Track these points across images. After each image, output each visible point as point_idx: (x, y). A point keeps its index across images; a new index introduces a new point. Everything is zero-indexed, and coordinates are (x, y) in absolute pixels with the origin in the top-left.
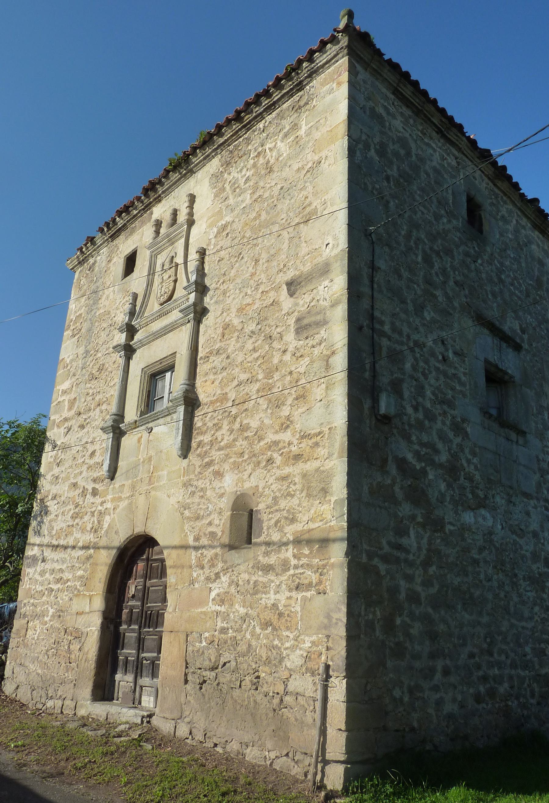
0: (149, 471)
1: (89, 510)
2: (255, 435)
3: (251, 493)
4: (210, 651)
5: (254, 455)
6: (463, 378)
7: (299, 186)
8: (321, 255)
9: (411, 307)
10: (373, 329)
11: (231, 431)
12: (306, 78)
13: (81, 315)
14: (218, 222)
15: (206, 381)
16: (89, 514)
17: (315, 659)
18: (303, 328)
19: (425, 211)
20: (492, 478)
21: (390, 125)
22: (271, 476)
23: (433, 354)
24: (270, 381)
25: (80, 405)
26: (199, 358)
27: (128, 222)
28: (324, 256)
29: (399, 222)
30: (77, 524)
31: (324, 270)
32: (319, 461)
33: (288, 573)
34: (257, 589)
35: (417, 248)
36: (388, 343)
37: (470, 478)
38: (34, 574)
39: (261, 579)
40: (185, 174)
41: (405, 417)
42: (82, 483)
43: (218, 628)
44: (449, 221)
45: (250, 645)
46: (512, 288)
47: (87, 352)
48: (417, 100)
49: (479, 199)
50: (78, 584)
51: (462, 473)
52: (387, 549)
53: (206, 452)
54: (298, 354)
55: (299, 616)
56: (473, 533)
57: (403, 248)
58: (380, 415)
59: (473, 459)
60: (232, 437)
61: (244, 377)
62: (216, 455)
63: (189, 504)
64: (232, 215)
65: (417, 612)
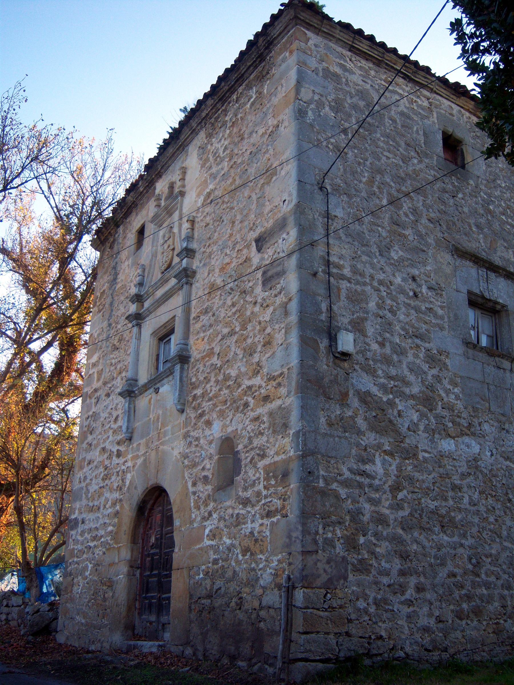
0: (158, 428)
1: (115, 471)
2: (234, 383)
3: (232, 436)
4: (206, 581)
5: (235, 402)
6: (440, 312)
7: (263, 151)
8: (280, 211)
9: (374, 249)
10: (329, 274)
11: (217, 382)
13: (104, 291)
14: (204, 190)
15: (197, 339)
16: (115, 474)
17: (281, 575)
18: (268, 281)
19: (391, 156)
20: (478, 406)
21: (347, 80)
22: (247, 418)
23: (402, 291)
24: (245, 332)
25: (106, 375)
26: (191, 318)
28: (282, 212)
29: (359, 170)
30: (107, 485)
31: (281, 225)
32: (281, 400)
33: (260, 503)
34: (239, 521)
35: (381, 192)
36: (348, 285)
37: (450, 408)
38: (76, 535)
39: (241, 512)
41: (368, 353)
42: (108, 446)
43: (211, 560)
44: (420, 162)
45: (235, 571)
46: (504, 217)
47: (110, 325)
48: (376, 52)
49: (459, 134)
51: (440, 403)
52: (347, 474)
53: (199, 404)
54: (265, 305)
55: (268, 539)
56: (454, 459)
57: (364, 194)
58: (339, 353)
59: (453, 389)
60: (218, 387)
61: (226, 331)
62: (206, 405)
63: (187, 453)
64: (214, 182)
65: (385, 533)
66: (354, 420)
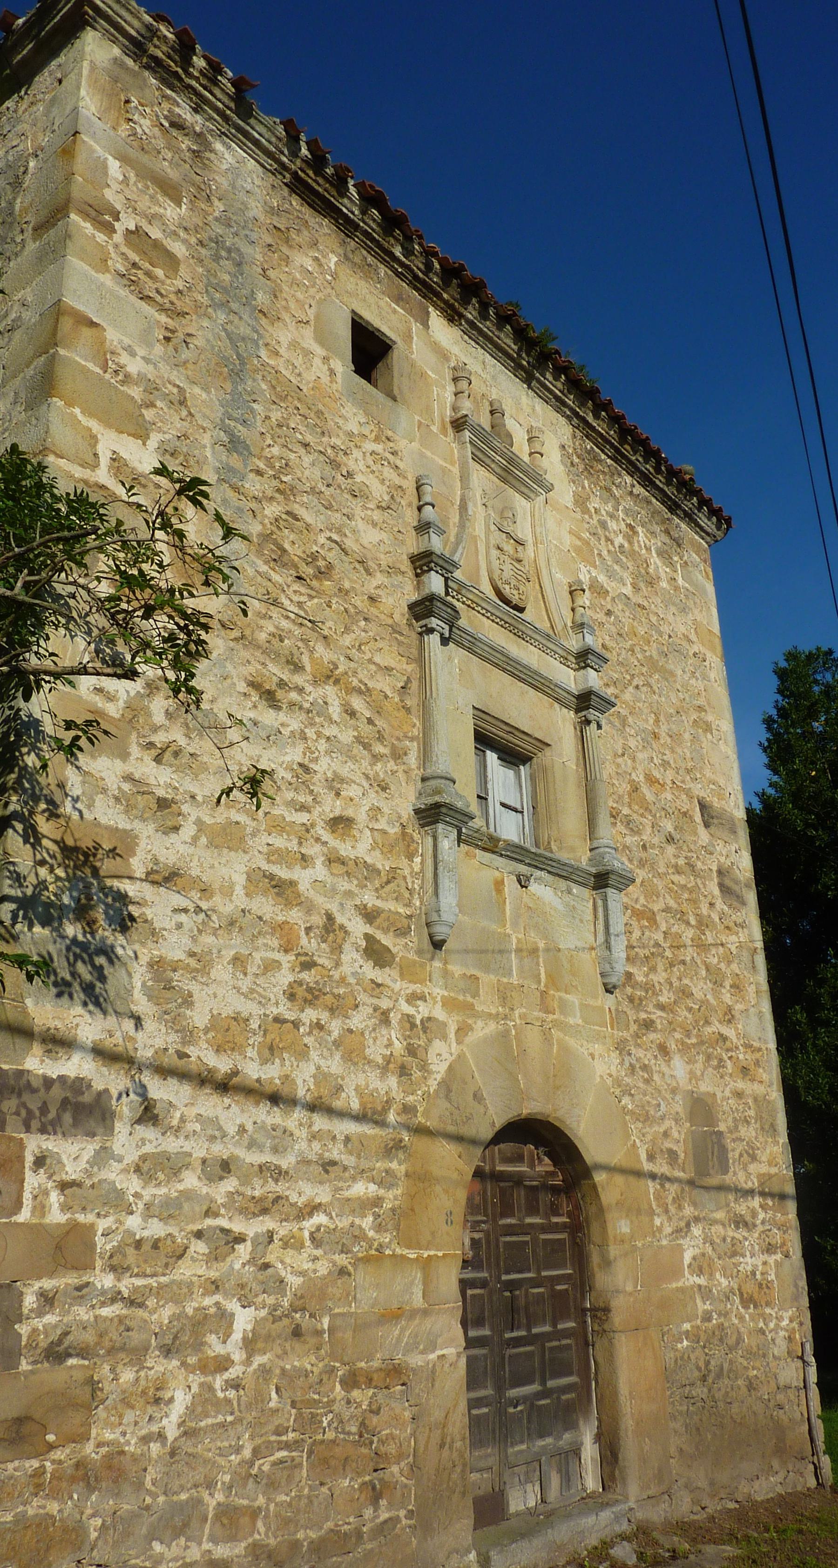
12: (684, 511)
27: (366, 234)
40: (521, 367)
43: (700, 1313)
50: (367, 1222)
66: (476, 1255)
